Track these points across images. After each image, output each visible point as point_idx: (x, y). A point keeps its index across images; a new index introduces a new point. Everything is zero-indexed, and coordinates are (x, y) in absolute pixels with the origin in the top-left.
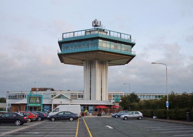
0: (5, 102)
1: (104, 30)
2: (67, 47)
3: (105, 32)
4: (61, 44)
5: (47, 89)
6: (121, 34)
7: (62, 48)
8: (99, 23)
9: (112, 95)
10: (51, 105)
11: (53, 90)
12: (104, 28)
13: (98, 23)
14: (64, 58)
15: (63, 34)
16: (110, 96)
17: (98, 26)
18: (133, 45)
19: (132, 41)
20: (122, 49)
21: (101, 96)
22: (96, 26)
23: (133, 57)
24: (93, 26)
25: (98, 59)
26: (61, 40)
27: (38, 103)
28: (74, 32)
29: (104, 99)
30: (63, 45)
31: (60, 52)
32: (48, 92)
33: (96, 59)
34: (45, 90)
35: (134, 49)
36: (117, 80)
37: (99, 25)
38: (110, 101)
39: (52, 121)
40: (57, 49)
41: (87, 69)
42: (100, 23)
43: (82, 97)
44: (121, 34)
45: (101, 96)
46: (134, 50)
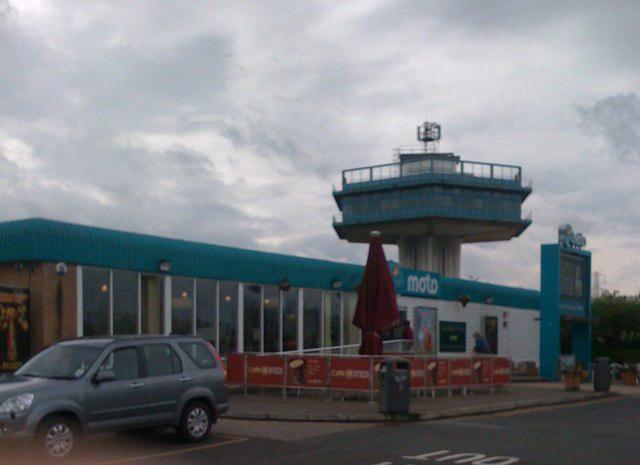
1: (458, 158)
4: (339, 197)
15: (344, 172)
18: (524, 194)
20: (479, 207)
22: (427, 140)
23: (525, 225)
24: (419, 139)
26: (339, 188)
28: (371, 168)
30: (345, 200)
31: (339, 219)
44: (492, 165)
46: (528, 208)
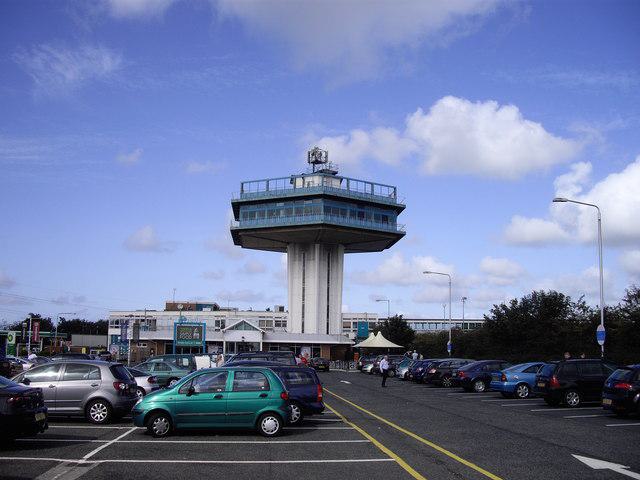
0: (105, 333)
2: (252, 215)
3: (337, 178)
4: (237, 207)
5: (206, 306)
6: (348, 180)
7: (241, 215)
8: (324, 154)
9: (352, 321)
10: (221, 344)
11: (216, 308)
12: (334, 170)
13: (321, 154)
14: (244, 239)
16: (346, 326)
17: (320, 162)
18: (399, 209)
19: (399, 202)
21: (303, 306)
22: (317, 162)
23: (400, 236)
25: (320, 241)
26: (237, 197)
27: (196, 340)
29: (311, 328)
31: (237, 225)
32: (207, 312)
33: (316, 241)
34: (199, 307)
35: (401, 219)
36: (377, 288)
37: (323, 160)
38: (347, 336)
39: (566, 405)
40: (229, 220)
41: (297, 263)
42: (326, 157)
43: (285, 325)
44: (372, 184)
45: (303, 306)
46: (402, 221)
